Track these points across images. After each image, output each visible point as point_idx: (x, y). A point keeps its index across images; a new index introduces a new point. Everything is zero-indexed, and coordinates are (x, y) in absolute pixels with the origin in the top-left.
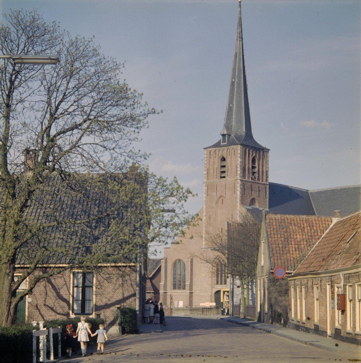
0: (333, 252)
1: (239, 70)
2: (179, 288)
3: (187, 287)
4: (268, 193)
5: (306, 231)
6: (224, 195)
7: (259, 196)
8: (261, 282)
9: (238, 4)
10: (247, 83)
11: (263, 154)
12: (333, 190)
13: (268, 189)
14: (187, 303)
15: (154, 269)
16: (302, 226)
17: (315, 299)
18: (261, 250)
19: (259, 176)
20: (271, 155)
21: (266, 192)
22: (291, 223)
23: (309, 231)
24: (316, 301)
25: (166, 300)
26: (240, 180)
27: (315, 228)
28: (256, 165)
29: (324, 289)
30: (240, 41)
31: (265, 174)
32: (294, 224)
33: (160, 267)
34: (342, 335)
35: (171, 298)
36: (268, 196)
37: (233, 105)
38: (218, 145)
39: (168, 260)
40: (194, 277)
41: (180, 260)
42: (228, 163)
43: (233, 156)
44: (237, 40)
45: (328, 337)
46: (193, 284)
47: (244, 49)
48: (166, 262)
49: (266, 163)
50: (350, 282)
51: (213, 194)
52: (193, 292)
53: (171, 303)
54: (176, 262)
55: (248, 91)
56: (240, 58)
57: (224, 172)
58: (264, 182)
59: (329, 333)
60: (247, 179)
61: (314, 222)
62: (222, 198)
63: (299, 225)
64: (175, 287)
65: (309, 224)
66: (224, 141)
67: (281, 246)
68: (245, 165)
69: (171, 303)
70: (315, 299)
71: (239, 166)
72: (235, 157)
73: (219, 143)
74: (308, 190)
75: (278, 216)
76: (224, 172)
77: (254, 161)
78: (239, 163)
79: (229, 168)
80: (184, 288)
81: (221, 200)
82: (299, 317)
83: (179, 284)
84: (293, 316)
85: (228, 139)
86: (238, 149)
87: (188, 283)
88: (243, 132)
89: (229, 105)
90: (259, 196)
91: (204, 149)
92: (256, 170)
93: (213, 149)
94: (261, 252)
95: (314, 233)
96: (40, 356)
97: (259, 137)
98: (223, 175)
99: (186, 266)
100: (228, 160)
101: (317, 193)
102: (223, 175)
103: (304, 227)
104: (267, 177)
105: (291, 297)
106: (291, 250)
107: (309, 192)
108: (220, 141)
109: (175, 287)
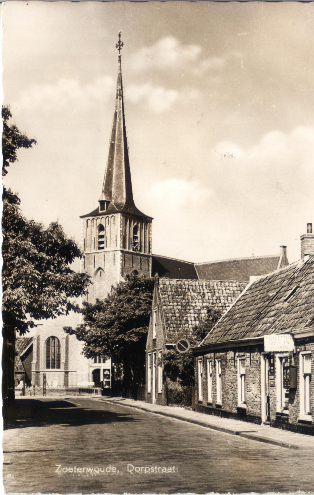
0: (261, 314)
1: (120, 131)
2: (53, 367)
3: (62, 366)
4: (151, 265)
5: (206, 298)
6: (102, 267)
7: (141, 269)
8: (152, 358)
9: (118, 58)
10: (129, 145)
11: (146, 224)
12: (221, 263)
13: (151, 261)
14: (62, 382)
15: (25, 348)
16: (202, 291)
17: (238, 375)
18: (152, 320)
19: (141, 247)
20: (154, 225)
21: (149, 265)
22: (189, 289)
23: (210, 298)
24: (239, 378)
25: (39, 379)
26: (120, 250)
27: (217, 295)
28: (138, 235)
29: (257, 361)
30: (120, 99)
31: (147, 245)
32: (193, 290)
33: (32, 345)
34: (290, 422)
35: (45, 378)
36: (150, 268)
37: (112, 169)
38: (95, 214)
39: (40, 337)
40: (69, 355)
41: (53, 338)
42: (107, 232)
43: (112, 225)
44: (117, 98)
45: (262, 424)
46: (69, 362)
47: (125, 108)
48: (38, 339)
49: (149, 234)
50: (307, 349)
51: (91, 266)
52: (69, 370)
53: (45, 382)
54: (49, 339)
55: (129, 155)
56: (120, 117)
57: (102, 243)
58: (147, 254)
59: (264, 418)
60: (127, 250)
61: (216, 288)
62: (101, 270)
63: (199, 291)
64: (48, 367)
65: (210, 290)
66: (102, 209)
67: (177, 315)
68: (125, 235)
69: (45, 382)
70: (238, 375)
71: (119, 236)
72: (115, 225)
73: (97, 210)
74: (193, 263)
75: (174, 282)
76: (102, 243)
77: (135, 232)
78: (119, 232)
79: (108, 238)
80: (59, 367)
81: (99, 272)
82: (210, 400)
83: (53, 362)
84: (201, 398)
85: (105, 208)
86: (118, 217)
87: (63, 360)
88: (18, 435)
89: (108, 169)
90: (141, 269)
91: (81, 217)
92: (138, 241)
93: (91, 218)
94: (152, 323)
95: (216, 300)
96: (172, 346)
97: (142, 204)
98: (102, 246)
99: (61, 344)
100: (107, 229)
101: (203, 265)
102: (102, 246)
103: (204, 294)
104: (150, 248)
105: (197, 374)
106: (189, 319)
107: (195, 265)
108: (98, 208)
109: (48, 367)
